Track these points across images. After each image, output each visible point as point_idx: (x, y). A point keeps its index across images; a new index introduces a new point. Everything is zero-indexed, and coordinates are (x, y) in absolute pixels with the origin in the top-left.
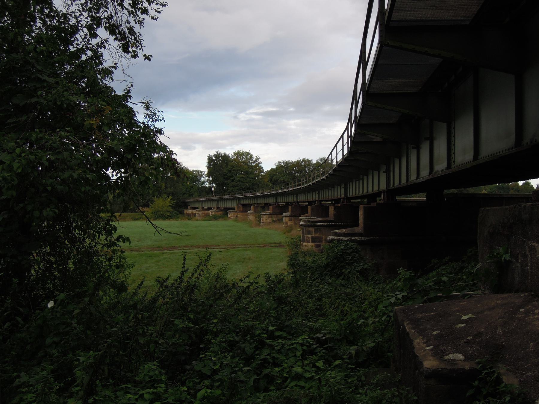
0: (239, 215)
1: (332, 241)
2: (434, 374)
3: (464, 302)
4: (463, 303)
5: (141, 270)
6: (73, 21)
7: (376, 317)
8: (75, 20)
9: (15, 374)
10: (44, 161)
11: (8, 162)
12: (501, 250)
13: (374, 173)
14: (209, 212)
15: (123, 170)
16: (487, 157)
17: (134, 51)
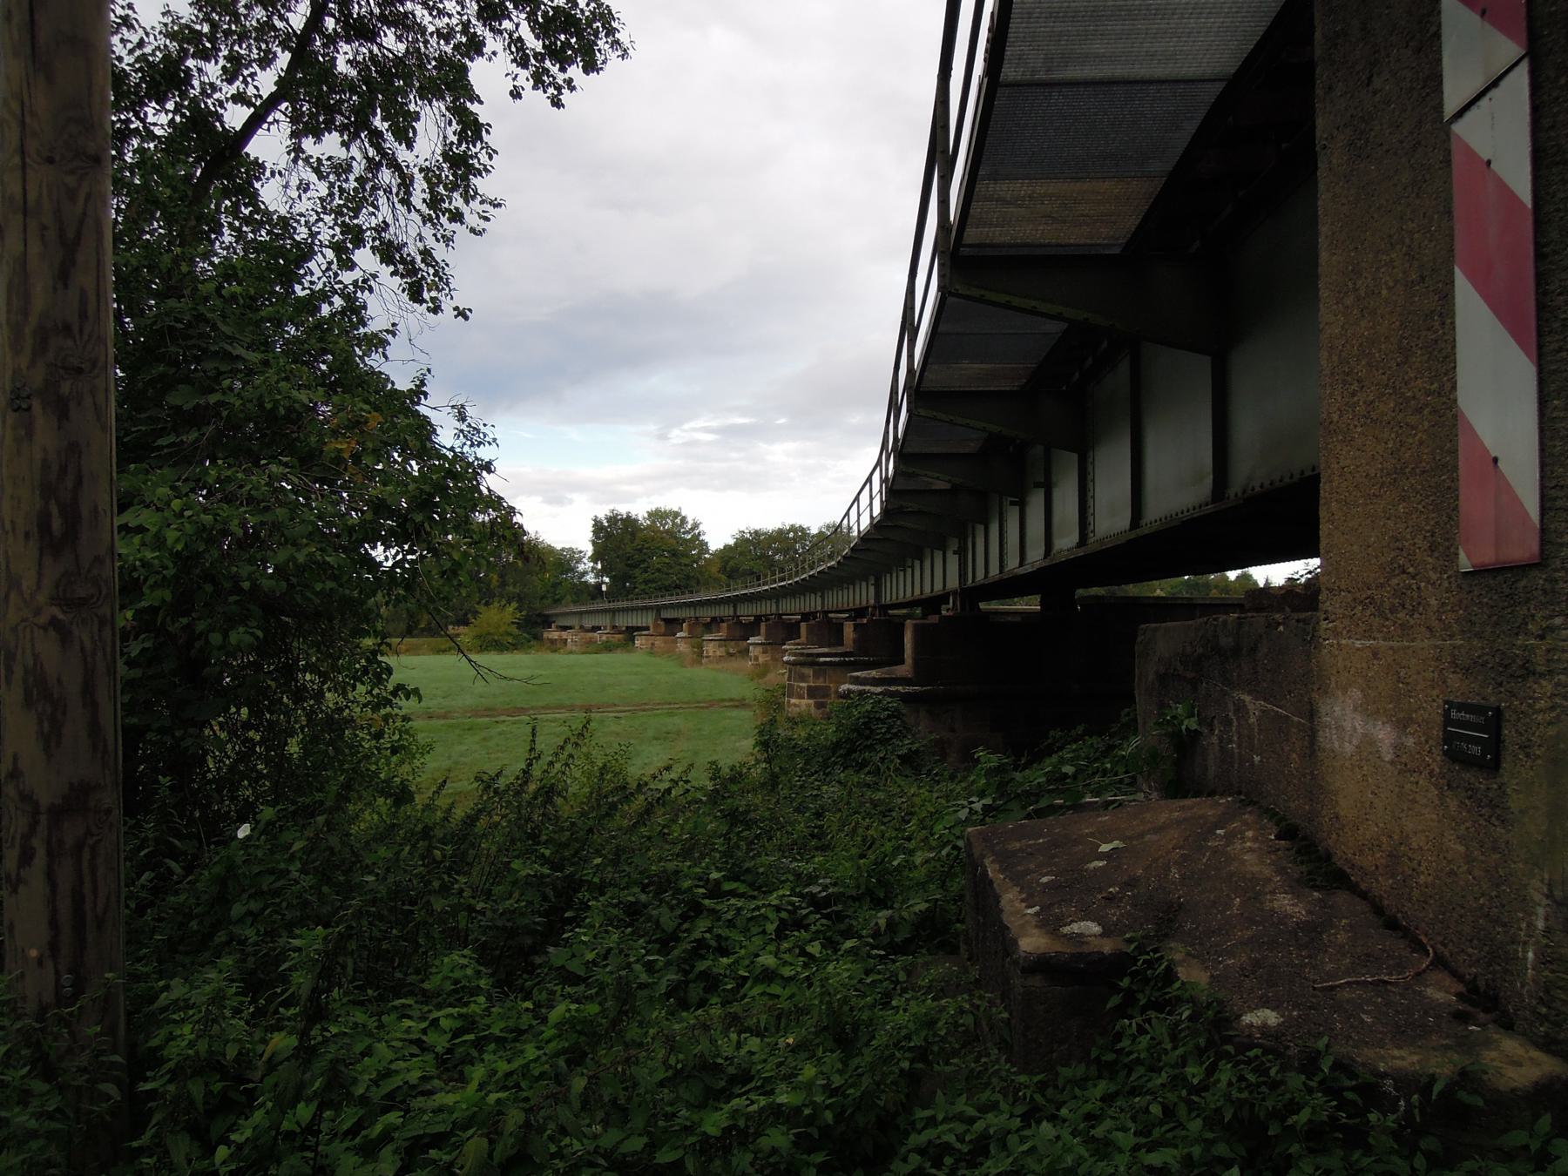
0: (659, 641)
1: (846, 695)
2: (1042, 965)
5: (449, 758)
6: (302, 234)
7: (931, 849)
8: (306, 231)
9: (161, 983)
10: (234, 526)
11: (154, 530)
12: (1180, 709)
13: (935, 555)
14: (596, 635)
15: (406, 547)
17: (433, 299)
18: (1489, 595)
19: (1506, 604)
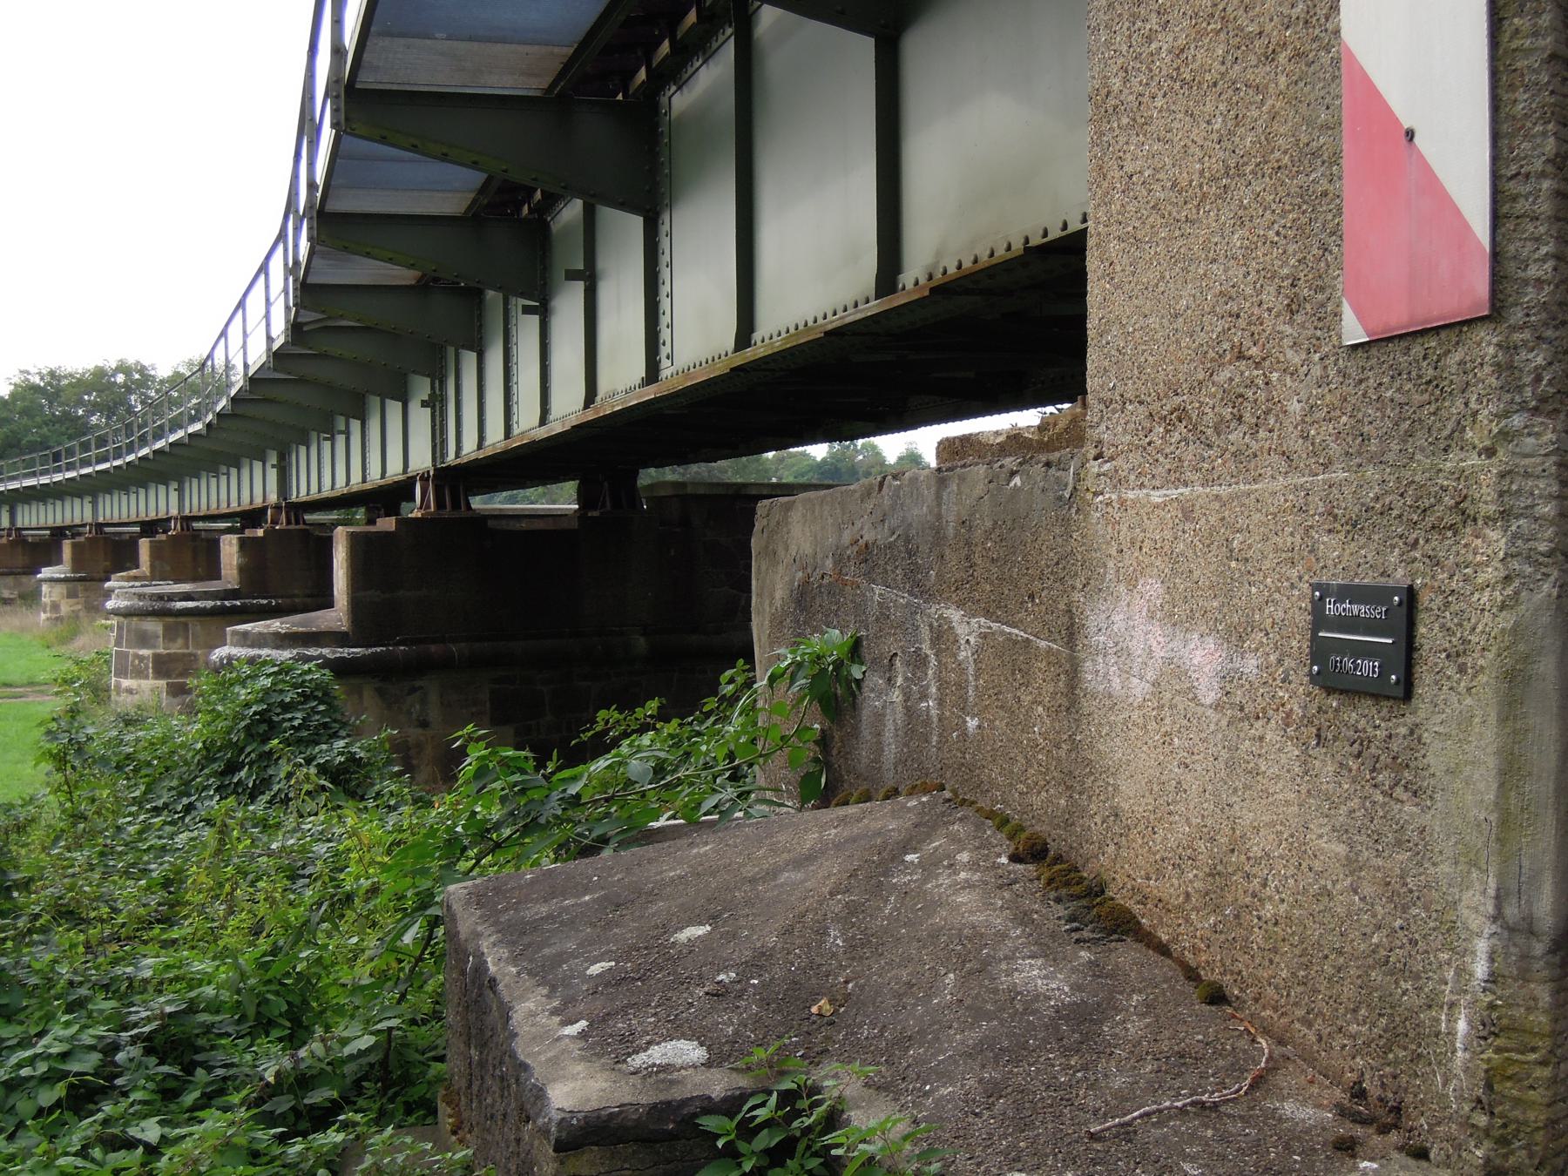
3: (706, 843)
4: (703, 850)
16: (784, 335)
18: (1397, 384)
19: (1426, 397)
